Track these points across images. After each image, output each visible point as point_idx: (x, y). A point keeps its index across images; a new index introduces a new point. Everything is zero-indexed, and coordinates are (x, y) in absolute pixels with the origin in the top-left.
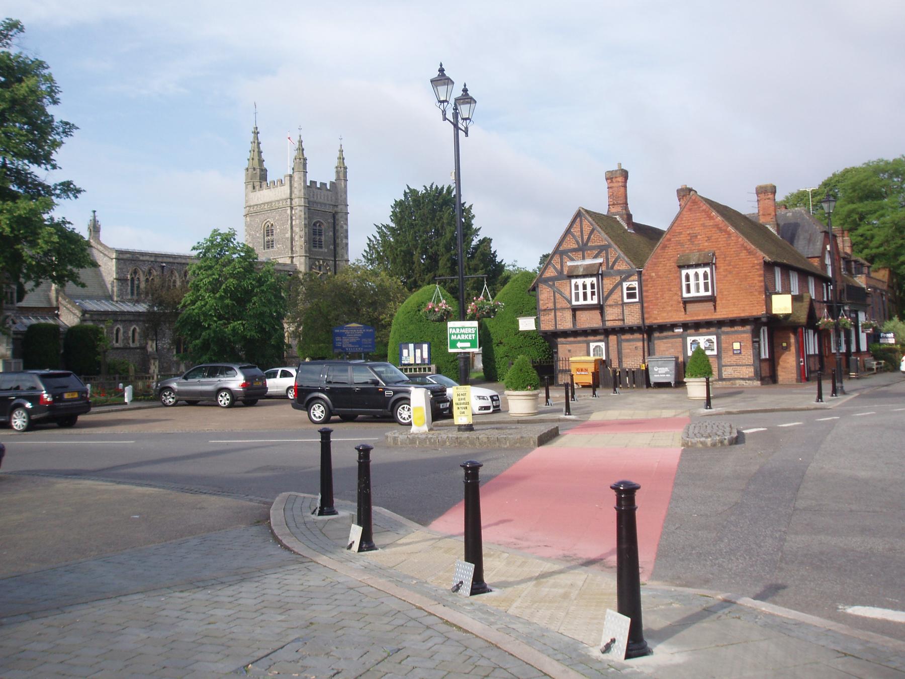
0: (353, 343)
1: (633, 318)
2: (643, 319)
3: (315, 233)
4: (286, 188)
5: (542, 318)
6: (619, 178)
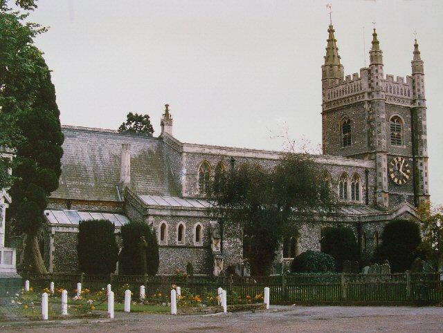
3: (393, 129)
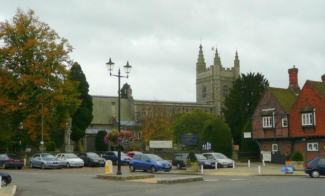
0: (189, 141)
1: (285, 135)
2: (289, 134)
4: (211, 72)
5: (254, 133)
6: (294, 66)
